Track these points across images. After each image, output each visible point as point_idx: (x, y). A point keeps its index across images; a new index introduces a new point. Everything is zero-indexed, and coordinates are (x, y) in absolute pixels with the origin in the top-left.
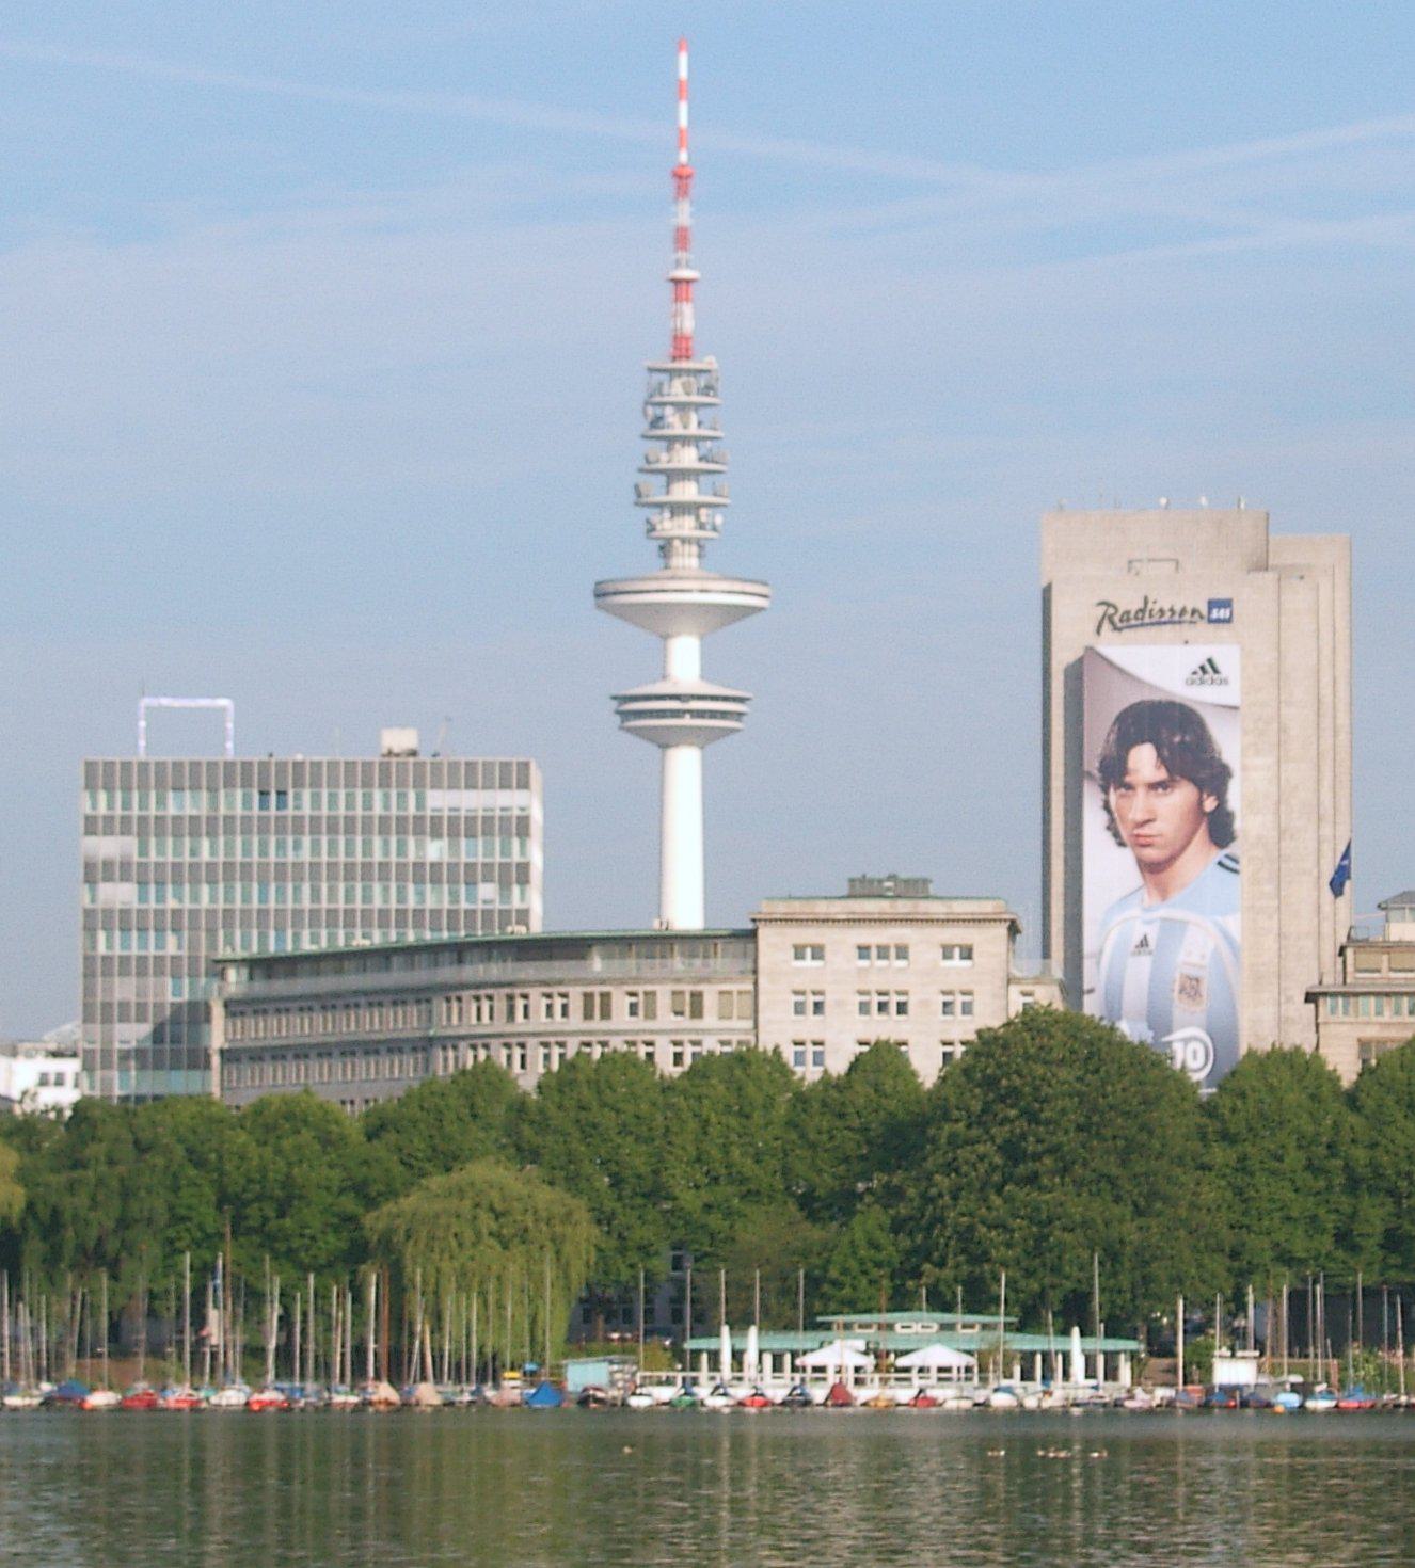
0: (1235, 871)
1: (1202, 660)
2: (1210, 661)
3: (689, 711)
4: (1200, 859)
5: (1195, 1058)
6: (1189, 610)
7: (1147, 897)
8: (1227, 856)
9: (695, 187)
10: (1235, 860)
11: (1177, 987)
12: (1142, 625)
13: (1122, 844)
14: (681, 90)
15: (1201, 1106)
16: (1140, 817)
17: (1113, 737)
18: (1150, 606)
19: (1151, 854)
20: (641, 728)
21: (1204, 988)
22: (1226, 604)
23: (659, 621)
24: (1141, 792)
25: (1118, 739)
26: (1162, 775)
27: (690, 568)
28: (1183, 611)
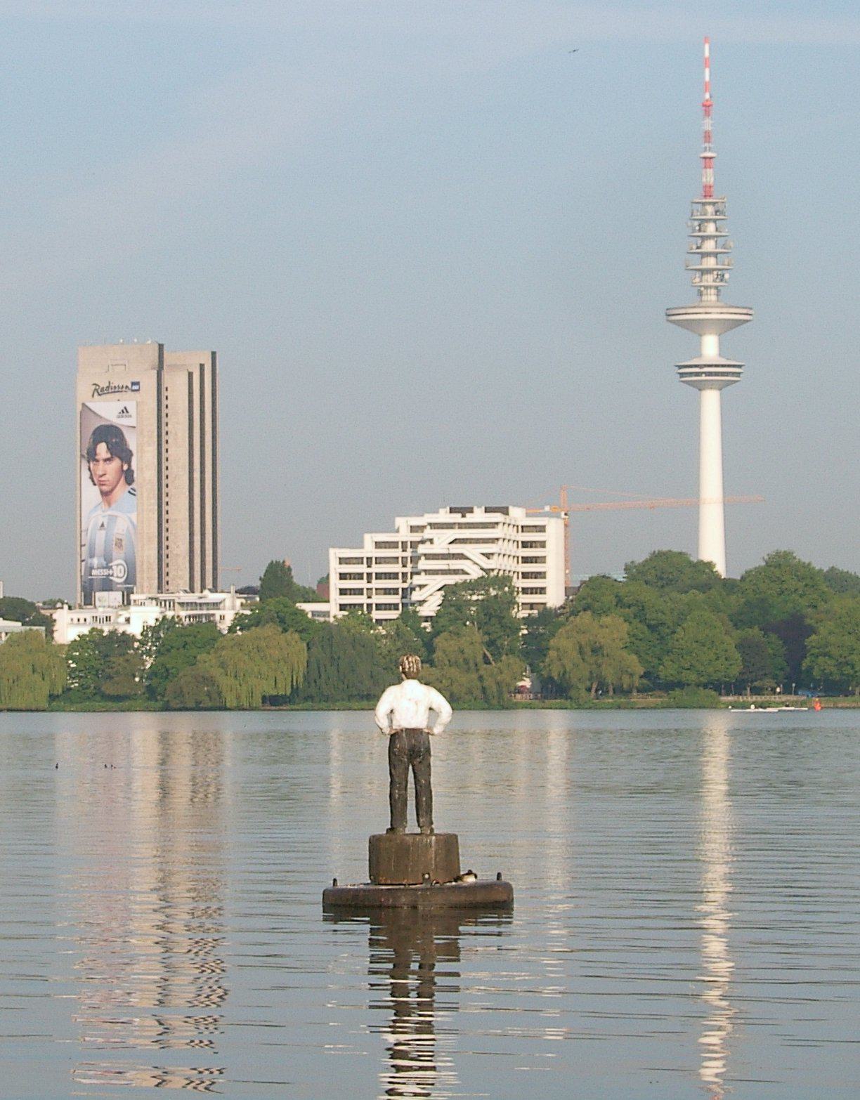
0: (134, 495)
1: (123, 408)
2: (125, 408)
3: (705, 373)
4: (122, 491)
5: (121, 572)
6: (125, 386)
7: (104, 506)
8: (132, 489)
9: (713, 110)
10: (134, 490)
11: (114, 543)
12: (108, 393)
13: (95, 485)
14: (707, 63)
15: (741, 581)
16: (101, 473)
17: (92, 440)
18: (111, 385)
19: (105, 488)
20: (689, 381)
21: (124, 543)
22: (138, 383)
23: (697, 328)
24: (101, 462)
25: (94, 441)
26: (109, 456)
27: (711, 301)
28: (123, 387)
